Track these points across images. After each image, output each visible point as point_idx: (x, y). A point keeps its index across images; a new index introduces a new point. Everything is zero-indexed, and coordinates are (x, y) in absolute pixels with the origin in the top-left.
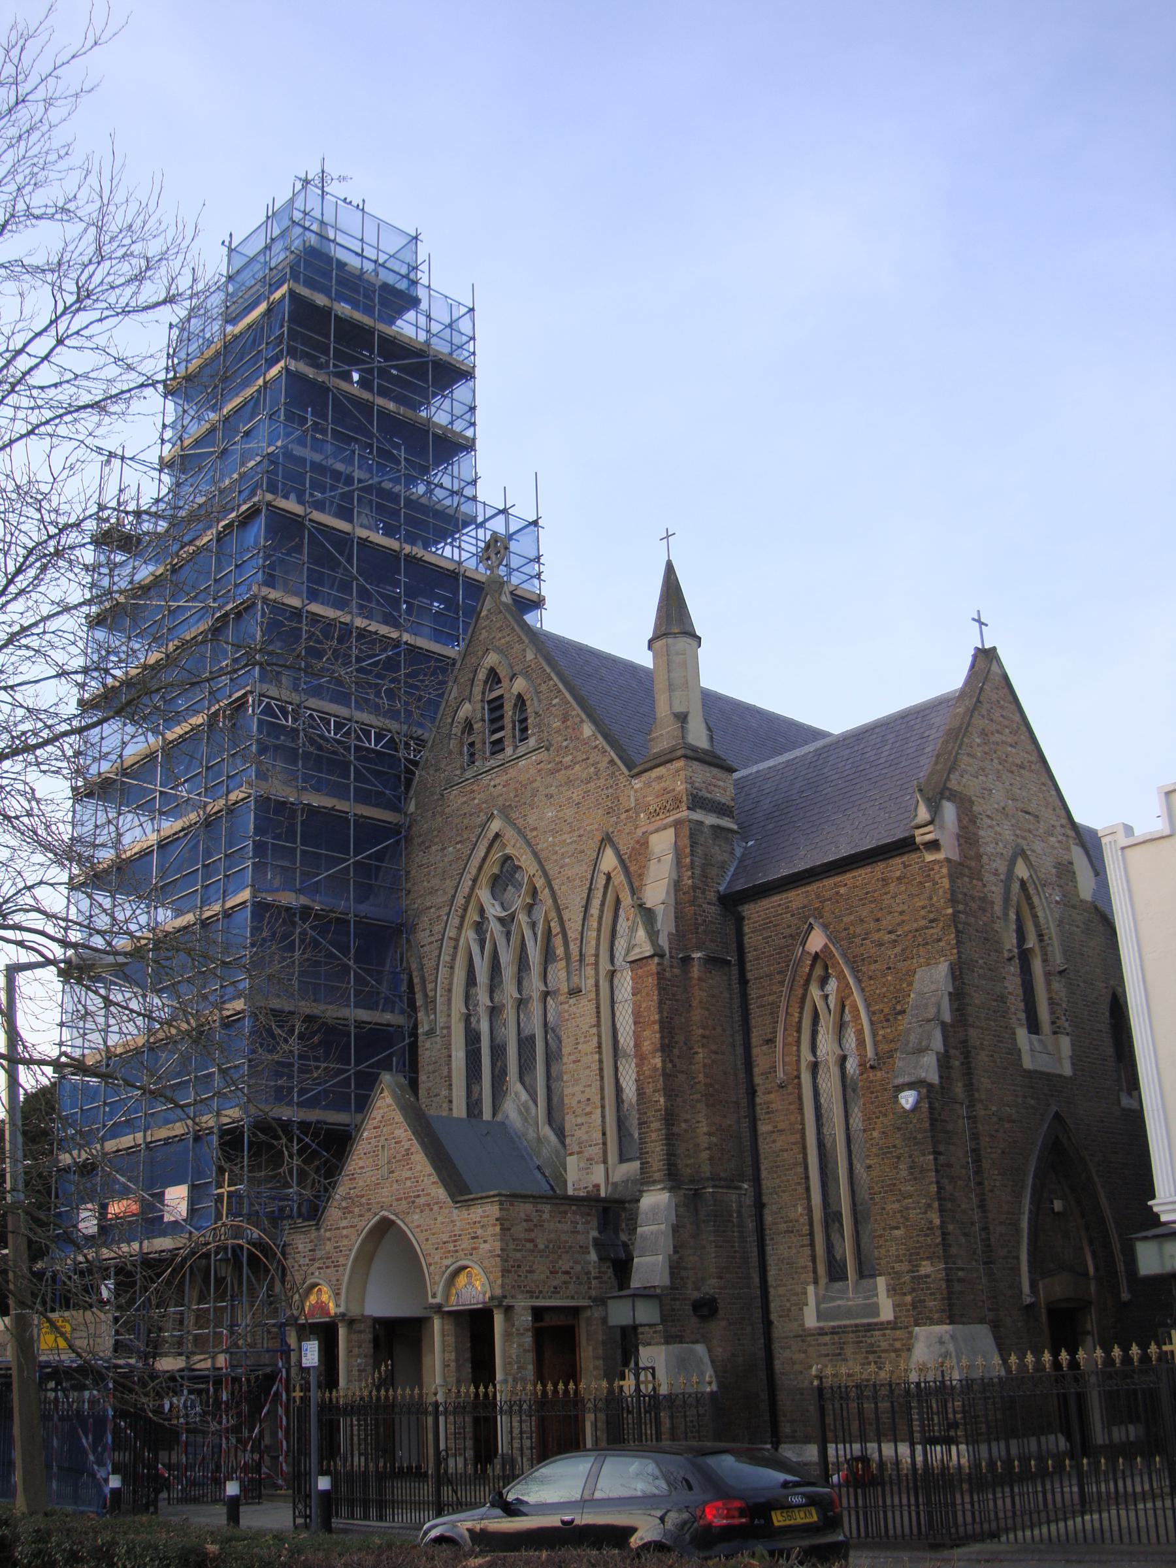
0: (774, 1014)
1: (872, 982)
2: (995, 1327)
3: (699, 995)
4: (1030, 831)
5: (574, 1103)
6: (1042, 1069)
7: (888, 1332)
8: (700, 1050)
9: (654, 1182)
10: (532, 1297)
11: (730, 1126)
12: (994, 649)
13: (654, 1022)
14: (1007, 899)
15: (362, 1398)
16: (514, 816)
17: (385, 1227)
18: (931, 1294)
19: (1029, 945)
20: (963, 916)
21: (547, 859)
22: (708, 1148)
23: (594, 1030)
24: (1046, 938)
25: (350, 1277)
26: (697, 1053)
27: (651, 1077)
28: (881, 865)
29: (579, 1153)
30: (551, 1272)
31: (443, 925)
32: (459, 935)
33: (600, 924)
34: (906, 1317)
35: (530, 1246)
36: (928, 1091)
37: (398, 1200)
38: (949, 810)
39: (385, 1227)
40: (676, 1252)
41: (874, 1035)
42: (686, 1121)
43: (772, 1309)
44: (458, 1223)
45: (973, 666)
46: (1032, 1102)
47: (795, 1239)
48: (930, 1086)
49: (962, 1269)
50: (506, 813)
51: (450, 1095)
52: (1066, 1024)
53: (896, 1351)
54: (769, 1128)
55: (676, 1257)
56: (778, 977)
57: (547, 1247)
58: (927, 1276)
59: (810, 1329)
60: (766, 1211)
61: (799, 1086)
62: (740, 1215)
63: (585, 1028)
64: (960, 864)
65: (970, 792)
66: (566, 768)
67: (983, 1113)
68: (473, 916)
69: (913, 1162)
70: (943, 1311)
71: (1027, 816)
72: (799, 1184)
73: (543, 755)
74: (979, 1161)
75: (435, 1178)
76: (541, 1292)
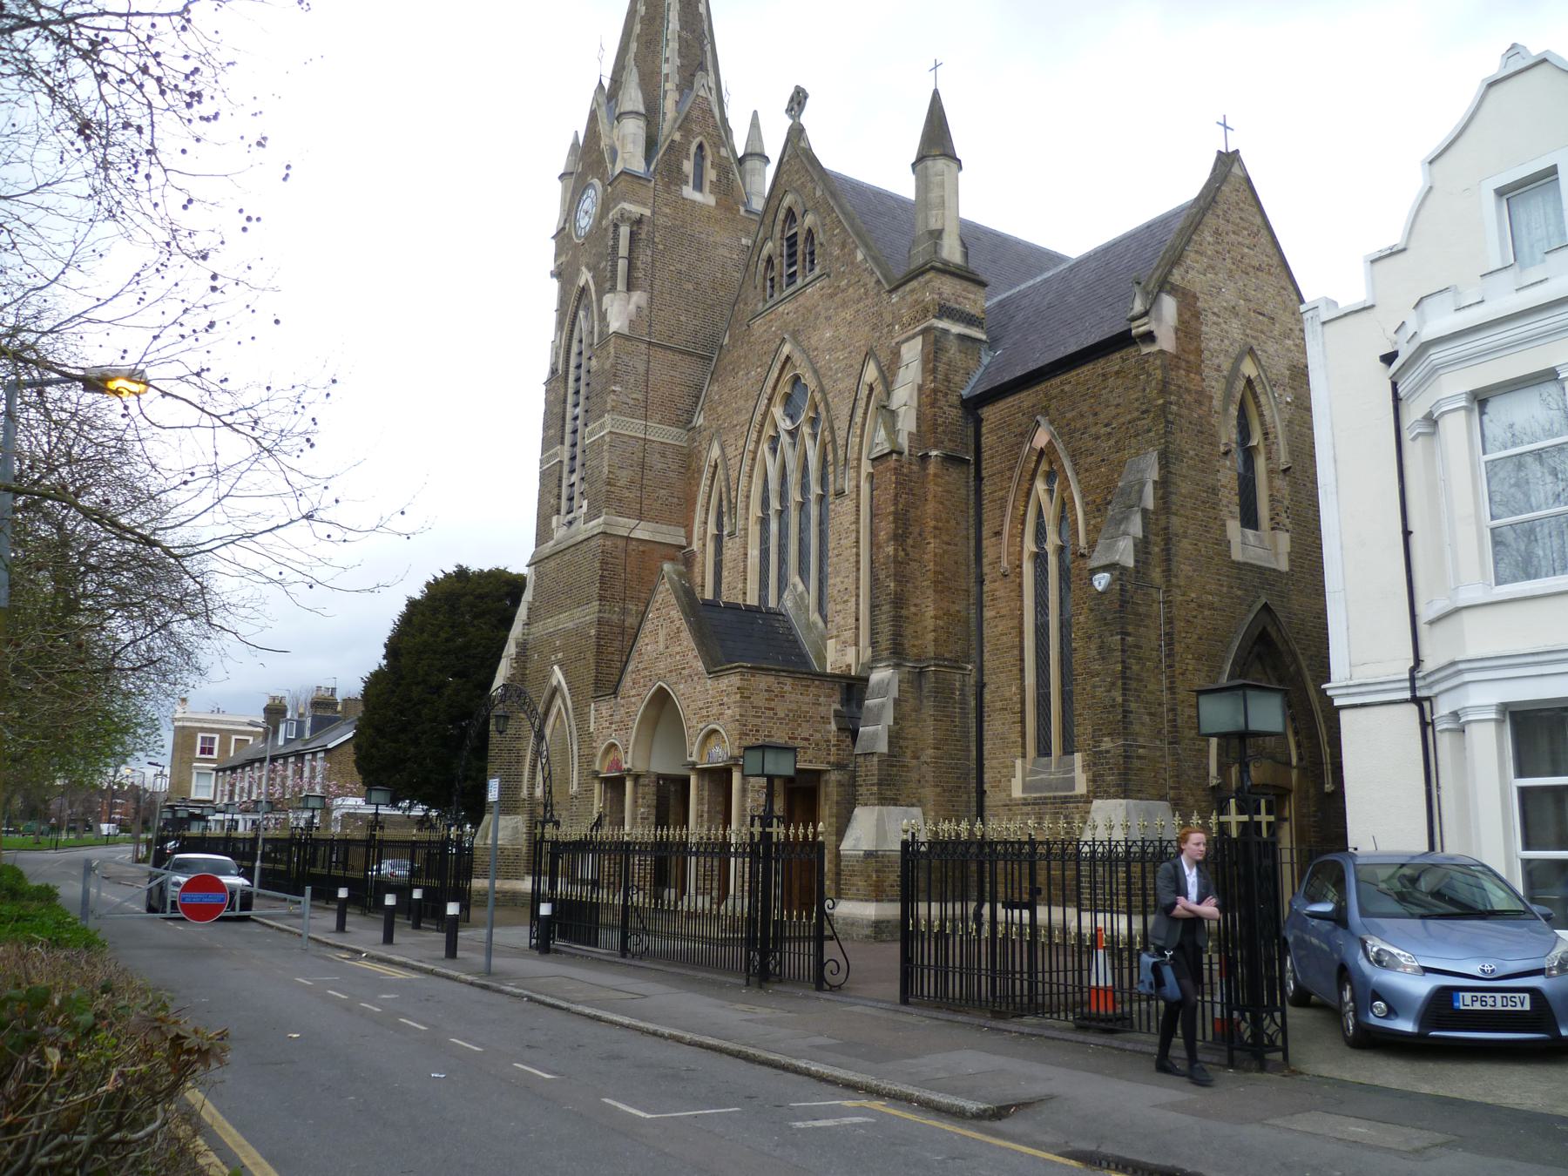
0: (1003, 508)
9: (881, 661)
14: (1228, 395)
19: (1254, 443)
20: (1174, 408)
28: (1102, 361)
38: (1169, 305)
41: (1087, 524)
45: (1214, 169)
48: (1124, 568)
50: (795, 335)
52: (1287, 521)
54: (993, 613)
56: (1008, 474)
58: (1107, 752)
61: (1021, 575)
62: (963, 694)
63: (847, 525)
64: (1177, 357)
65: (1197, 288)
73: (825, 282)
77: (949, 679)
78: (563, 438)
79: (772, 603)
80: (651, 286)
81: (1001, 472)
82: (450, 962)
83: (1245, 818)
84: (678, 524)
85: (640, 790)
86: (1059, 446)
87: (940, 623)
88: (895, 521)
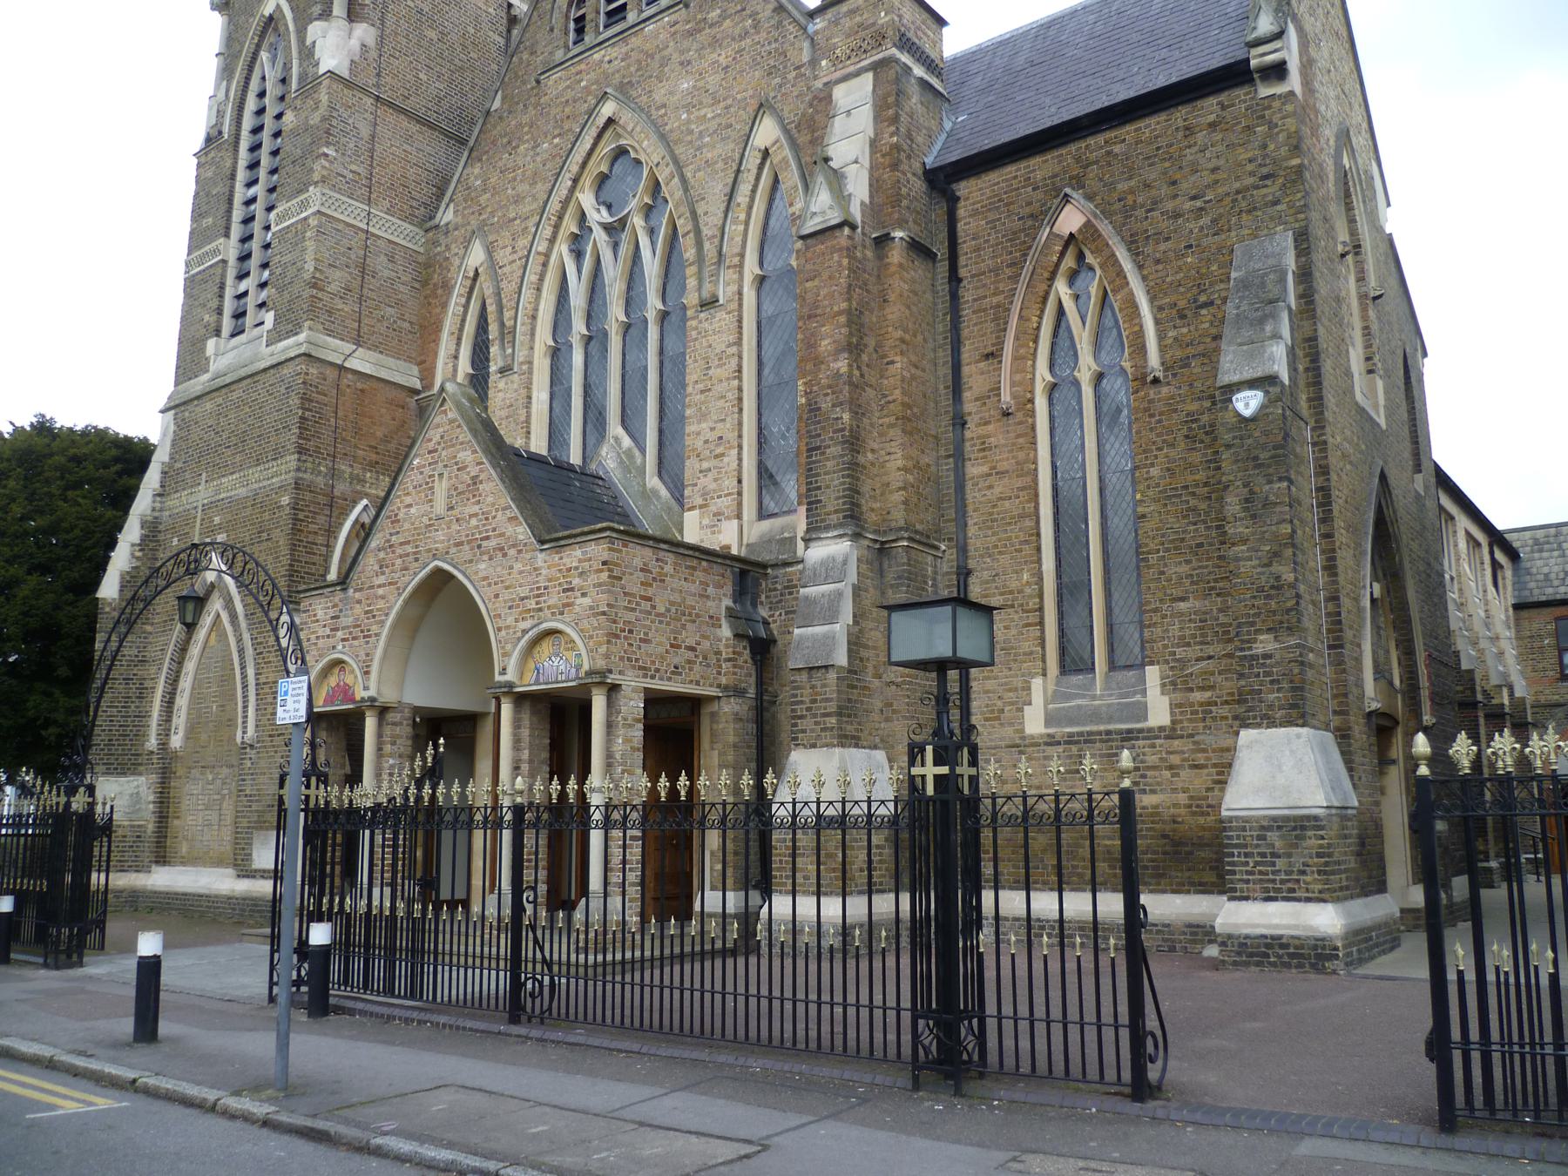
1: (1160, 267)
3: (898, 285)
5: (699, 444)
7: (1158, 742)
8: (898, 358)
9: (827, 528)
10: (645, 676)
13: (840, 313)
15: (392, 800)
16: (634, 94)
17: (439, 583)
18: (1272, 682)
25: (385, 651)
26: (892, 362)
27: (830, 387)
29: (701, 507)
30: (672, 646)
31: (530, 238)
34: (1190, 720)
35: (646, 605)
37: (457, 545)
39: (439, 583)
40: (856, 622)
41: (1161, 337)
42: (873, 451)
43: (973, 711)
44: (544, 572)
47: (1016, 617)
50: (623, 88)
53: (1171, 768)
55: (857, 629)
57: (668, 610)
58: (1267, 656)
59: (1032, 737)
60: (972, 580)
63: (720, 347)
66: (711, 26)
68: (570, 225)
69: (1252, 492)
75: (515, 511)
76: (657, 670)
77: (922, 564)
78: (228, 228)
79: (575, 458)
80: (382, 20)
81: (995, 271)
82: (144, 1052)
83: (944, 770)
84: (409, 359)
85: (388, 730)
86: (1105, 228)
87: (910, 478)
88: (849, 323)
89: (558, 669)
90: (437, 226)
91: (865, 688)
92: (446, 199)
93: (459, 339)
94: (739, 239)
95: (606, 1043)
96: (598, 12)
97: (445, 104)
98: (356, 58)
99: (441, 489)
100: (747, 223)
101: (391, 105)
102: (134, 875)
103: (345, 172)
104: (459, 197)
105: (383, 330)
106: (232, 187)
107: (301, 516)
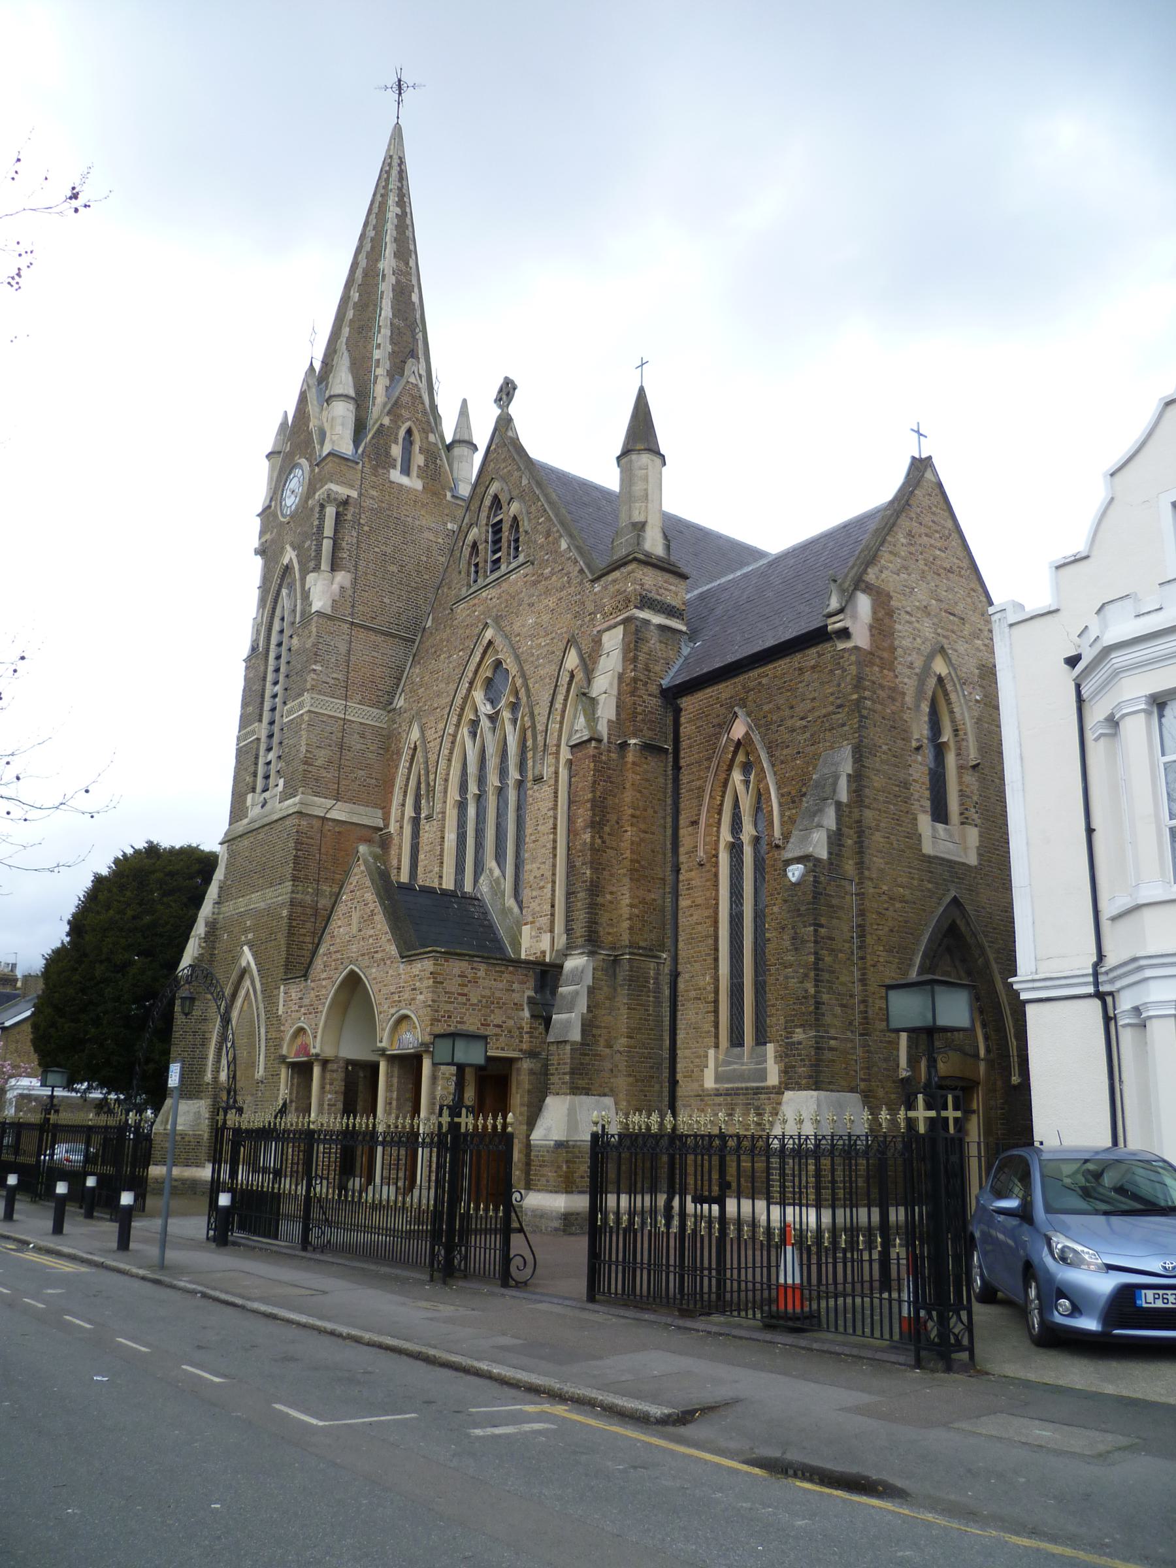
0: (700, 798)
2: (866, 1096)
4: (953, 632)
6: (942, 855)
9: (576, 948)
11: (654, 900)
12: (930, 458)
13: (588, 801)
14: (920, 692)
20: (868, 703)
21: (526, 661)
22: (630, 919)
23: (551, 813)
24: (961, 733)
25: (326, 1022)
28: (799, 656)
29: (532, 923)
32: (456, 731)
33: (563, 717)
35: (463, 999)
36: (815, 865)
38: (864, 603)
41: (782, 815)
42: (611, 893)
46: (930, 886)
48: (818, 860)
49: (835, 1039)
50: (497, 620)
51: (441, 871)
54: (689, 902)
58: (800, 1043)
60: (680, 980)
61: (716, 865)
63: (544, 811)
64: (871, 653)
65: (890, 588)
66: (546, 579)
67: (872, 891)
69: (796, 933)
70: (810, 1077)
71: (952, 618)
72: (709, 955)
74: (864, 936)
75: (389, 936)
77: (643, 966)
78: (261, 715)
80: (356, 567)
81: (699, 762)
82: (121, 1254)
83: (456, 1120)
85: (328, 1076)
86: (756, 737)
87: (636, 911)
89: (410, 1040)
90: (394, 709)
91: (597, 1055)
92: (400, 690)
93: (405, 792)
94: (556, 734)
95: (331, 1260)
96: (486, 562)
97: (404, 617)
98: (336, 598)
99: (355, 917)
100: (561, 723)
101: (362, 626)
102: (195, 1169)
103: (328, 680)
104: (407, 689)
105: (356, 787)
106: (264, 686)
107: (294, 923)
